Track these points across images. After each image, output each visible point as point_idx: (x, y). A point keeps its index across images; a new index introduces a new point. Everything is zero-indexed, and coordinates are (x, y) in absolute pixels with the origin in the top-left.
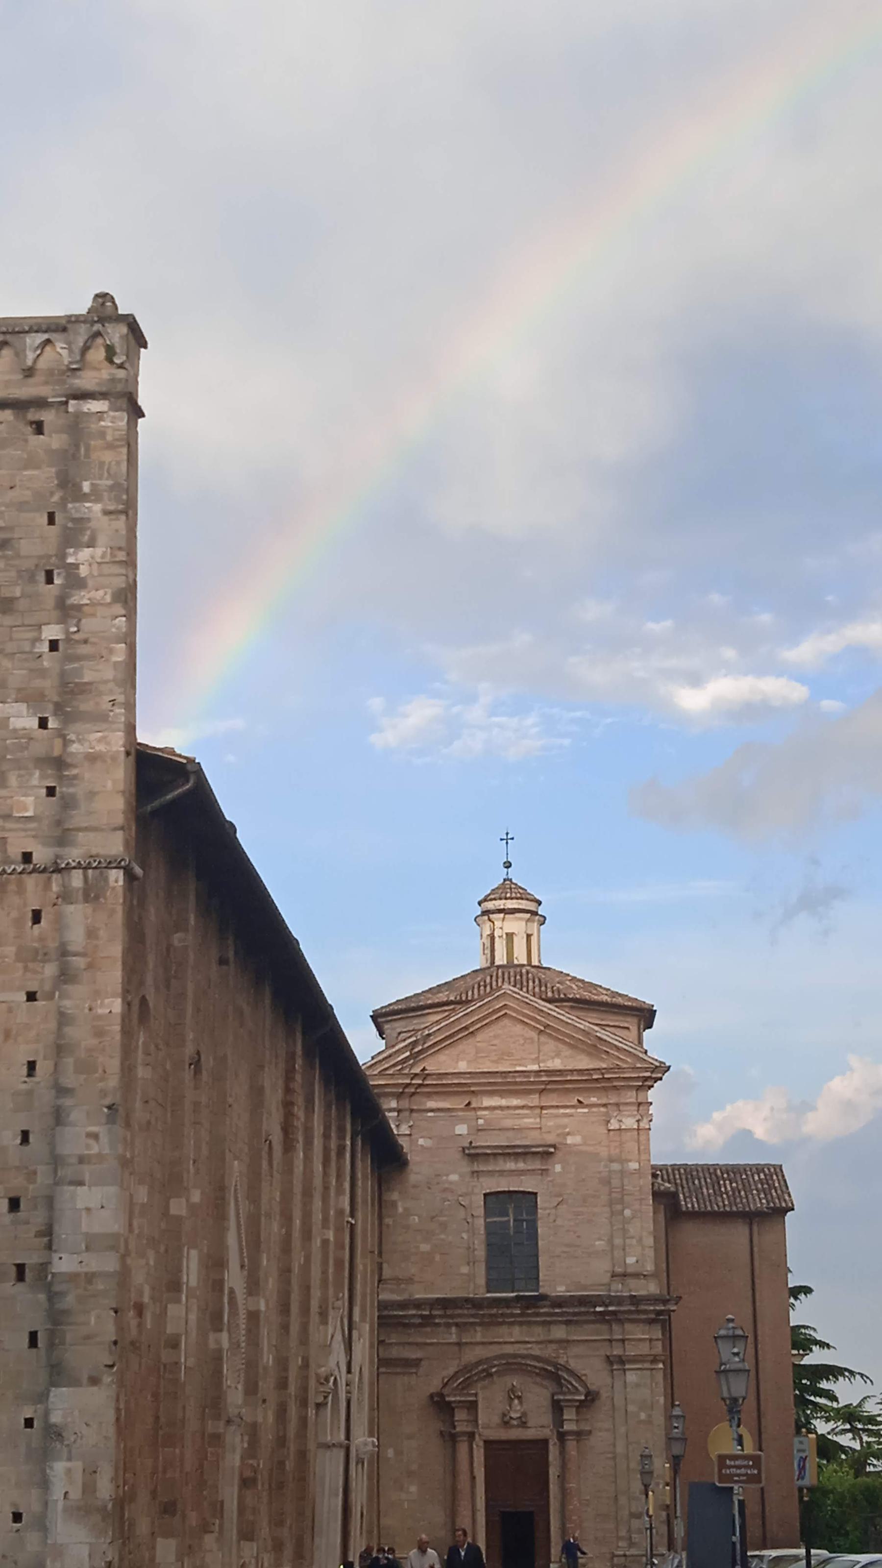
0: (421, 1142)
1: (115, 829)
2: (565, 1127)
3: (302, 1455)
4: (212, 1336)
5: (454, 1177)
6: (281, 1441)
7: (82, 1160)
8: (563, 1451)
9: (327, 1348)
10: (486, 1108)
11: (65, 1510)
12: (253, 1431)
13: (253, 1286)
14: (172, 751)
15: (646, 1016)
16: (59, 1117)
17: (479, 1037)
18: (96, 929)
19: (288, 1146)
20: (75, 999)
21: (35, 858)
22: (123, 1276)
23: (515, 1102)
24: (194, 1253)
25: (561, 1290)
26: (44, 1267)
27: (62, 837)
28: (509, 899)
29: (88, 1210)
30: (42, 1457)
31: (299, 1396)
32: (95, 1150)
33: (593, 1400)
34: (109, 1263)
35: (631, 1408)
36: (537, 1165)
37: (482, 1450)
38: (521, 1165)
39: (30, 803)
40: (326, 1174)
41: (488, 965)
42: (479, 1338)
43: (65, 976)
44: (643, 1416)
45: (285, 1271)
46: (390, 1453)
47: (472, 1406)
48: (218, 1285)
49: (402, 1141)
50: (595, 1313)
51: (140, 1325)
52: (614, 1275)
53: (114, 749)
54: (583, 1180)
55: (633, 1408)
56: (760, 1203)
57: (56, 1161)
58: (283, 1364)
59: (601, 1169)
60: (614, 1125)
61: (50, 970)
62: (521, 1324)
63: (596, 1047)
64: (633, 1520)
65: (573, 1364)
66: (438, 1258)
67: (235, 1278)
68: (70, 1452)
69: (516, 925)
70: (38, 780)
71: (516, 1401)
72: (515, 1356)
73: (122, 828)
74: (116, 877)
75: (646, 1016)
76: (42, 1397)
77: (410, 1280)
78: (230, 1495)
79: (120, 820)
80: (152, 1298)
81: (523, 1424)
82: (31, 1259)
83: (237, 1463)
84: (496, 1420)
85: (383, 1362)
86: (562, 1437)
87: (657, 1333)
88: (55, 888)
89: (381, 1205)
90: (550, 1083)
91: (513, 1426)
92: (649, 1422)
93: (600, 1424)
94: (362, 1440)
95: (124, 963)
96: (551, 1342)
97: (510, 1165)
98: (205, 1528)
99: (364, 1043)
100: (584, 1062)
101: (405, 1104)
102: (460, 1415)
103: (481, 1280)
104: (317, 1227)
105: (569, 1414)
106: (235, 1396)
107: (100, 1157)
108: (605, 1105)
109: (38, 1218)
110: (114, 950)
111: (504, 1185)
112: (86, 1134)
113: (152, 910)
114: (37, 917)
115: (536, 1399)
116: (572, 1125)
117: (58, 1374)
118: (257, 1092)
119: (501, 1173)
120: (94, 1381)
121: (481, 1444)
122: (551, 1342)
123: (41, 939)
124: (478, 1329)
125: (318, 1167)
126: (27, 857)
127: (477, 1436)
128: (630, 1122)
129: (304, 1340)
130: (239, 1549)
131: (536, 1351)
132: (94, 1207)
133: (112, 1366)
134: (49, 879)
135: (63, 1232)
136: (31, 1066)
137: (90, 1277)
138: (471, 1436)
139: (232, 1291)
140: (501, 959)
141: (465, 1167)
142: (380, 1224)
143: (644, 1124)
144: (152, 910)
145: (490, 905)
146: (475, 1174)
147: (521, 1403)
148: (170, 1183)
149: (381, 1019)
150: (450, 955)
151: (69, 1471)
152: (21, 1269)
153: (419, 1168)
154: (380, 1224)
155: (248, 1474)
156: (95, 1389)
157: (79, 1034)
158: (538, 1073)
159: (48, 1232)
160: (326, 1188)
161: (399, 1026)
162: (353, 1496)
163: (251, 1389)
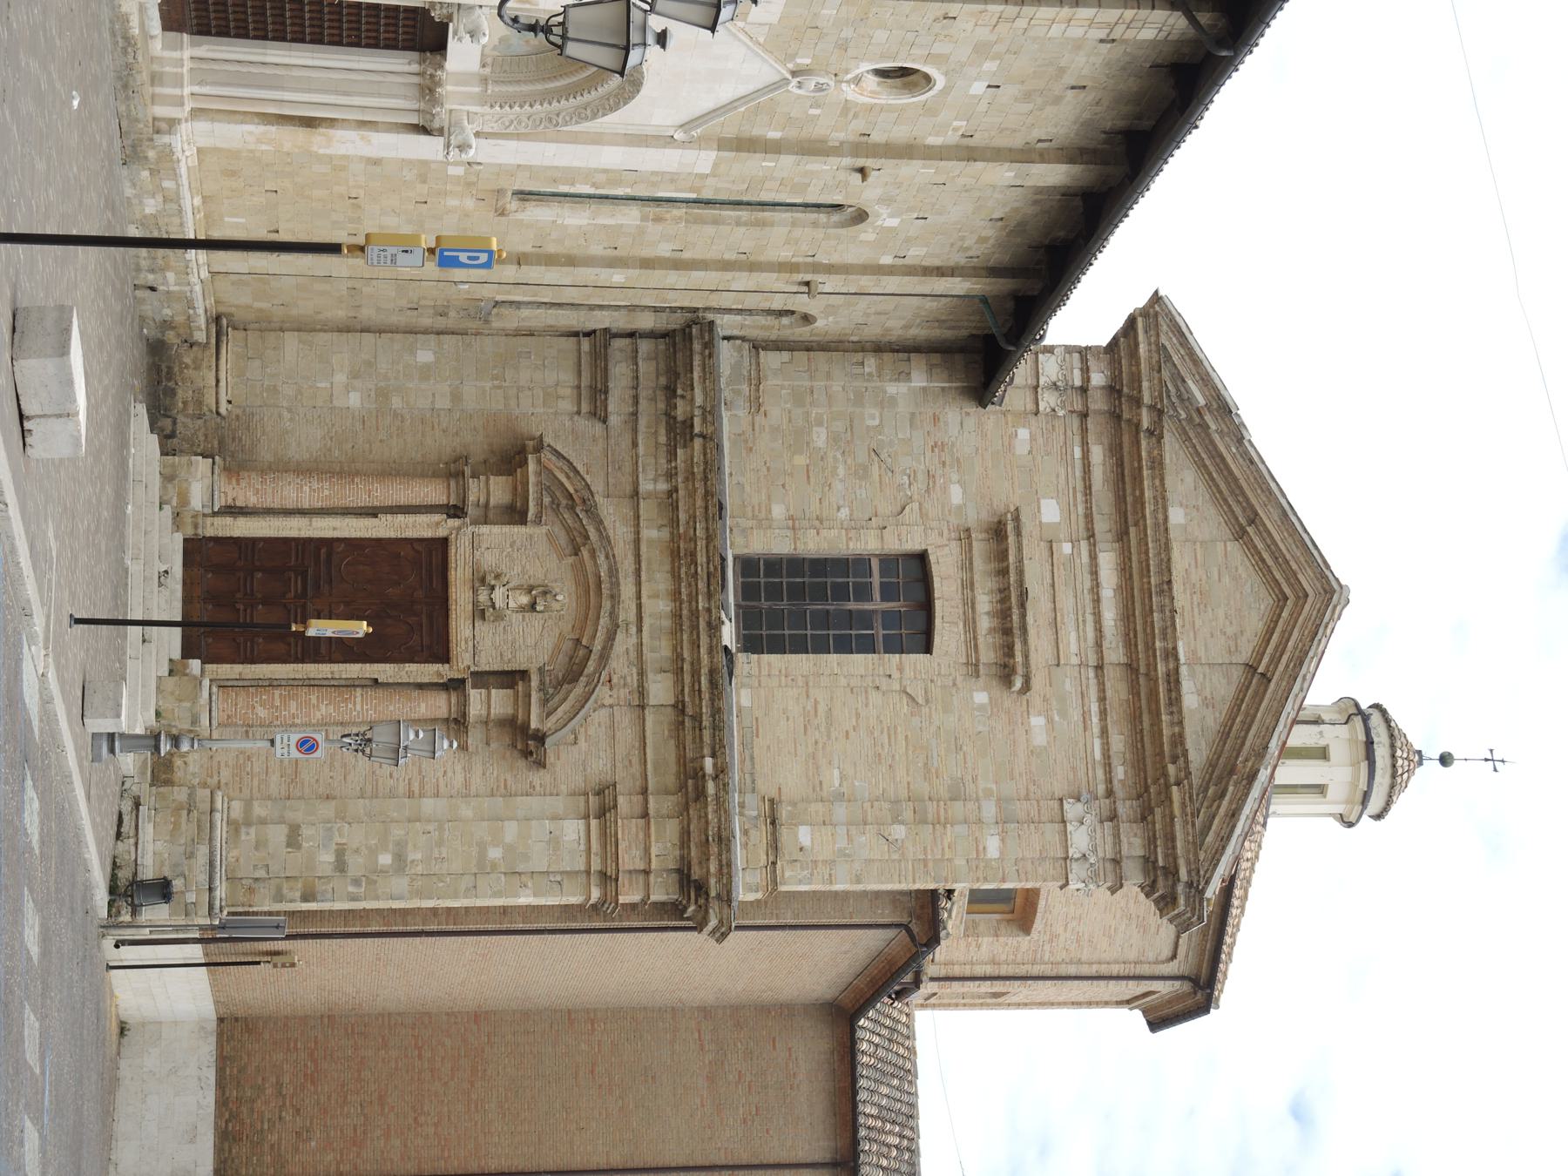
2: (1063, 714)
10: (1093, 557)
33: (526, 754)
37: (428, 534)
38: (984, 623)
42: (649, 533)
44: (495, 853)
47: (515, 514)
54: (959, 748)
60: (1072, 810)
62: (677, 616)
66: (801, 460)
71: (524, 600)
72: (615, 598)
77: (756, 405)
81: (479, 613)
84: (489, 560)
91: (475, 591)
96: (642, 674)
99: (1087, 315)
115: (528, 641)
116: (1061, 727)
122: (642, 674)
124: (665, 534)
127: (454, 523)
131: (624, 643)
141: (976, 516)
147: (522, 609)
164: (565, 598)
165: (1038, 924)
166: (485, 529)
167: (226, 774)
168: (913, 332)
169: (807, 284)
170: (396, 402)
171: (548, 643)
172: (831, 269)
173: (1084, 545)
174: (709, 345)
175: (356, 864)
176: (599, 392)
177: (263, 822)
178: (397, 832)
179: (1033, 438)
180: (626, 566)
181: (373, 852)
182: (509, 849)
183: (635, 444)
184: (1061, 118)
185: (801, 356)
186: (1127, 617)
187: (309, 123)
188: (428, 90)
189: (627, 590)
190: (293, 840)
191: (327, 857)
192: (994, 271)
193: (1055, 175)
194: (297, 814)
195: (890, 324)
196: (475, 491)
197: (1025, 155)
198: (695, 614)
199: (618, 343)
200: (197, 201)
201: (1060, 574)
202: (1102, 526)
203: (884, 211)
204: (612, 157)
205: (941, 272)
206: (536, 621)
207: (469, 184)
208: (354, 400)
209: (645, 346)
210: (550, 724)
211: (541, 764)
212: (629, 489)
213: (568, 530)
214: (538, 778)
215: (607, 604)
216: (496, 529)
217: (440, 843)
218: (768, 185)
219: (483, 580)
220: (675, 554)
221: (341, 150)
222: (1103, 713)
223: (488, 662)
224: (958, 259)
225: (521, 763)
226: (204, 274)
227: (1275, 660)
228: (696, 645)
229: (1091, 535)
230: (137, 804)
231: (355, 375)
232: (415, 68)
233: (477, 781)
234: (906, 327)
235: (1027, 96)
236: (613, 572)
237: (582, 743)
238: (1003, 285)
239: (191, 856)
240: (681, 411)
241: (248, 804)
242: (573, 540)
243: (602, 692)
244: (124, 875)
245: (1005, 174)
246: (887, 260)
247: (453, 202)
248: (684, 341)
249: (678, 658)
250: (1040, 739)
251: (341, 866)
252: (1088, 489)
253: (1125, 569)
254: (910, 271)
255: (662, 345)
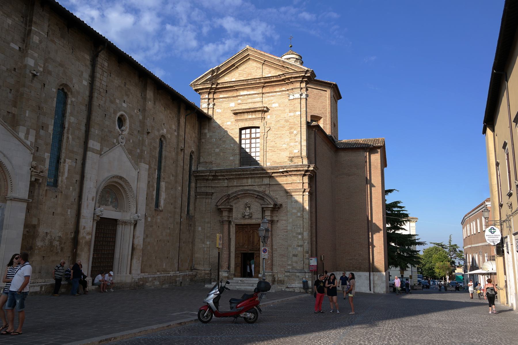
2: (272, 100)
5: (229, 123)
17: (240, 69)
33: (279, 208)
37: (234, 228)
38: (254, 116)
40: (280, 172)
42: (235, 184)
44: (299, 214)
47: (230, 210)
54: (279, 121)
59: (286, 116)
60: (291, 97)
62: (251, 178)
64: (294, 257)
66: (222, 154)
71: (248, 209)
72: (247, 190)
77: (211, 163)
81: (250, 217)
84: (240, 216)
85: (197, 194)
91: (246, 219)
96: (263, 185)
97: (250, 116)
103: (237, 162)
108: (288, 90)
115: (256, 207)
121: (234, 226)
122: (263, 185)
124: (235, 180)
127: (232, 223)
131: (257, 188)
138: (230, 222)
141: (233, 118)
147: (250, 209)
164: (247, 200)
165: (320, 116)
166: (234, 217)
167: (282, 269)
168: (196, 131)
169: (181, 150)
170: (209, 235)
171: (256, 204)
172: (178, 145)
173: (239, 98)
174: (198, 172)
175: (301, 243)
176: (207, 194)
177: (292, 262)
178: (294, 234)
179: (218, 109)
180: (241, 188)
181: (298, 239)
182: (298, 211)
183: (218, 187)
184: (135, 91)
185: (201, 154)
186: (253, 88)
187: (133, 249)
188: (125, 223)
189: (246, 188)
190: (295, 255)
191: (299, 249)
192: (179, 112)
193: (150, 94)
194: (291, 255)
195: (194, 136)
196: (226, 219)
197: (144, 99)
198: (251, 174)
199: (198, 190)
200: (158, 273)
201: (245, 102)
202: (235, 94)
203: (162, 131)
204: (143, 185)
205: (179, 123)
206: (252, 206)
207: (153, 217)
208: (208, 243)
209: (198, 185)
210: (272, 203)
211: (281, 205)
212: (226, 188)
213: (234, 200)
214: (284, 206)
215: (249, 192)
216: (234, 214)
217: (297, 225)
218: (154, 154)
219: (244, 217)
220: (239, 178)
221: (141, 242)
222: (272, 92)
223: (260, 216)
224: (176, 119)
225: (281, 209)
226: (178, 272)
227: (261, 59)
228: (257, 174)
230: (288, 287)
231: (203, 243)
232: (121, 226)
233: (284, 218)
234: (195, 133)
235: (128, 96)
236: (242, 190)
237: (277, 197)
238: (182, 111)
239: (299, 276)
240: (211, 178)
241: (289, 265)
242: (236, 199)
243: (267, 192)
244: (302, 290)
245: (150, 104)
246: (176, 133)
247: (159, 220)
248: (196, 176)
249: (259, 177)
251: (301, 246)
252: (228, 97)
253: (243, 89)
254: (178, 129)
255: (198, 182)
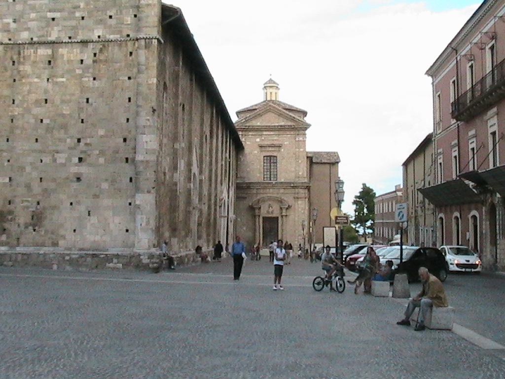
0: (248, 143)
1: (155, 27)
3: (215, 219)
4: (188, 185)
5: (256, 152)
6: (209, 214)
7: (144, 127)
8: (282, 220)
9: (222, 192)
11: (141, 229)
12: (201, 211)
13: (201, 172)
14: (172, 5)
15: (305, 114)
16: (137, 114)
18: (149, 59)
19: (211, 137)
20: (142, 78)
21: (131, 36)
22: (158, 163)
23: (272, 133)
24: (182, 161)
25: (283, 180)
26: (133, 160)
27: (138, 29)
28: (271, 85)
29: (146, 142)
30: (133, 215)
31: (214, 203)
32: (148, 124)
34: (153, 158)
35: (300, 210)
36: (277, 149)
38: (273, 149)
39: (129, 19)
41: (265, 100)
43: (139, 72)
45: (211, 171)
46: (239, 219)
48: (190, 171)
49: (243, 143)
50: (291, 186)
51: (165, 178)
52: (296, 177)
53: (155, 3)
55: (300, 210)
56: (333, 161)
57: (137, 127)
58: (210, 195)
60: (297, 139)
61: (135, 70)
63: (293, 119)
65: (285, 199)
67: (195, 169)
68: (142, 213)
69: (273, 91)
70: (132, 12)
73: (157, 27)
74: (155, 42)
75: (305, 114)
76: (134, 196)
78: (194, 226)
79: (156, 24)
80: (168, 171)
82: (130, 156)
83: (197, 219)
86: (282, 216)
87: (306, 191)
88: (136, 45)
89: (237, 159)
90: (281, 129)
92: (304, 213)
93: (291, 213)
94: (232, 215)
95: (157, 68)
97: (270, 149)
98: (186, 236)
99: (234, 119)
100: (290, 124)
101: (244, 133)
102: (257, 211)
104: (219, 161)
105: (284, 211)
106: (195, 199)
107: (150, 126)
109: (132, 144)
110: (154, 63)
111: (269, 154)
112: (145, 118)
113: (168, 58)
114: (131, 53)
116: (286, 140)
117: (138, 189)
118: (202, 120)
119: (268, 151)
120: (149, 192)
123: (132, 60)
125: (220, 145)
126: (128, 36)
128: (301, 139)
129: (216, 188)
130: (198, 242)
132: (148, 142)
133: (154, 188)
134: (135, 43)
135: (139, 149)
136: (130, 99)
137: (147, 162)
138: (259, 216)
139: (194, 174)
140: (269, 99)
141: (258, 149)
142: (237, 163)
143: (305, 139)
144: (168, 58)
145: (265, 85)
146: (261, 151)
148: (175, 139)
149: (238, 113)
150: (255, 97)
151: (142, 218)
152: (127, 159)
153: (247, 150)
154: (237, 163)
155: (200, 222)
156: (148, 194)
157: (144, 89)
158: (278, 126)
159: (135, 148)
160: (222, 151)
161: (242, 115)
162: (229, 230)
163: (200, 200)
229: (261, 135)
250: (288, 143)
